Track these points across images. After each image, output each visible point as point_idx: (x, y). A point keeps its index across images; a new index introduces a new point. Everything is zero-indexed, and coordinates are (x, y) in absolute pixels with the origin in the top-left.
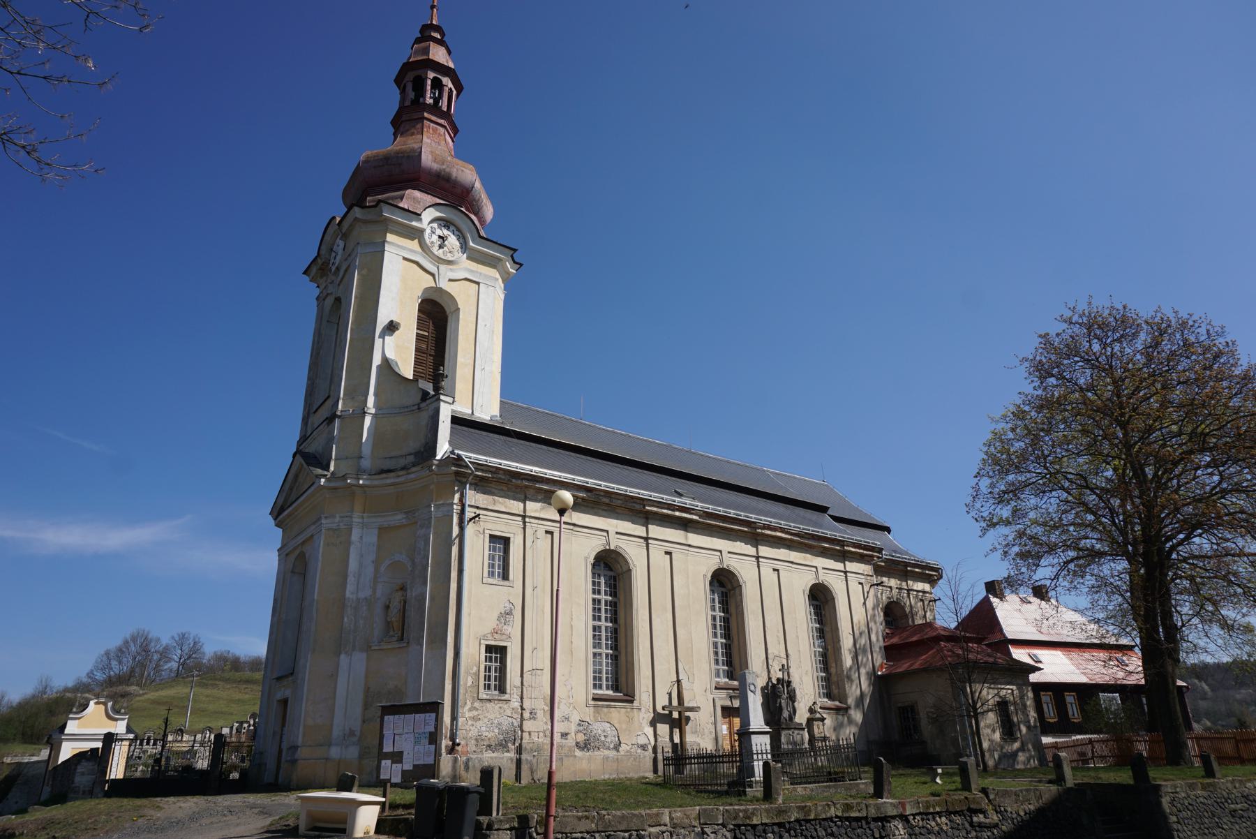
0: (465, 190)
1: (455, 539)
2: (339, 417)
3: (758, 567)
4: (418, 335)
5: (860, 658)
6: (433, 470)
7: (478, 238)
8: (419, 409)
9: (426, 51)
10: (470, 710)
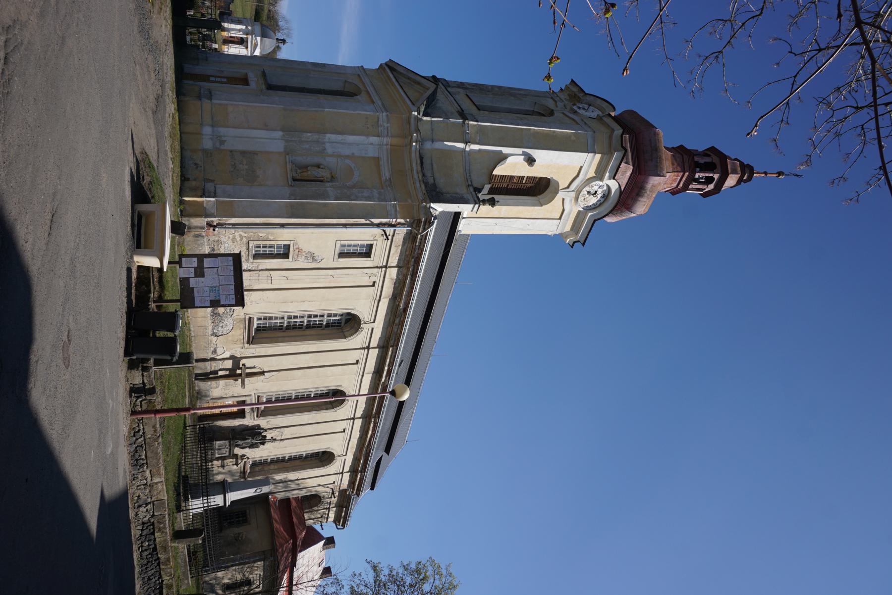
0: (630, 206)
1: (370, 221)
2: (464, 122)
3: (347, 419)
4: (523, 177)
5: (281, 485)
6: (422, 203)
7: (593, 220)
8: (469, 185)
9: (734, 172)
10: (240, 236)
